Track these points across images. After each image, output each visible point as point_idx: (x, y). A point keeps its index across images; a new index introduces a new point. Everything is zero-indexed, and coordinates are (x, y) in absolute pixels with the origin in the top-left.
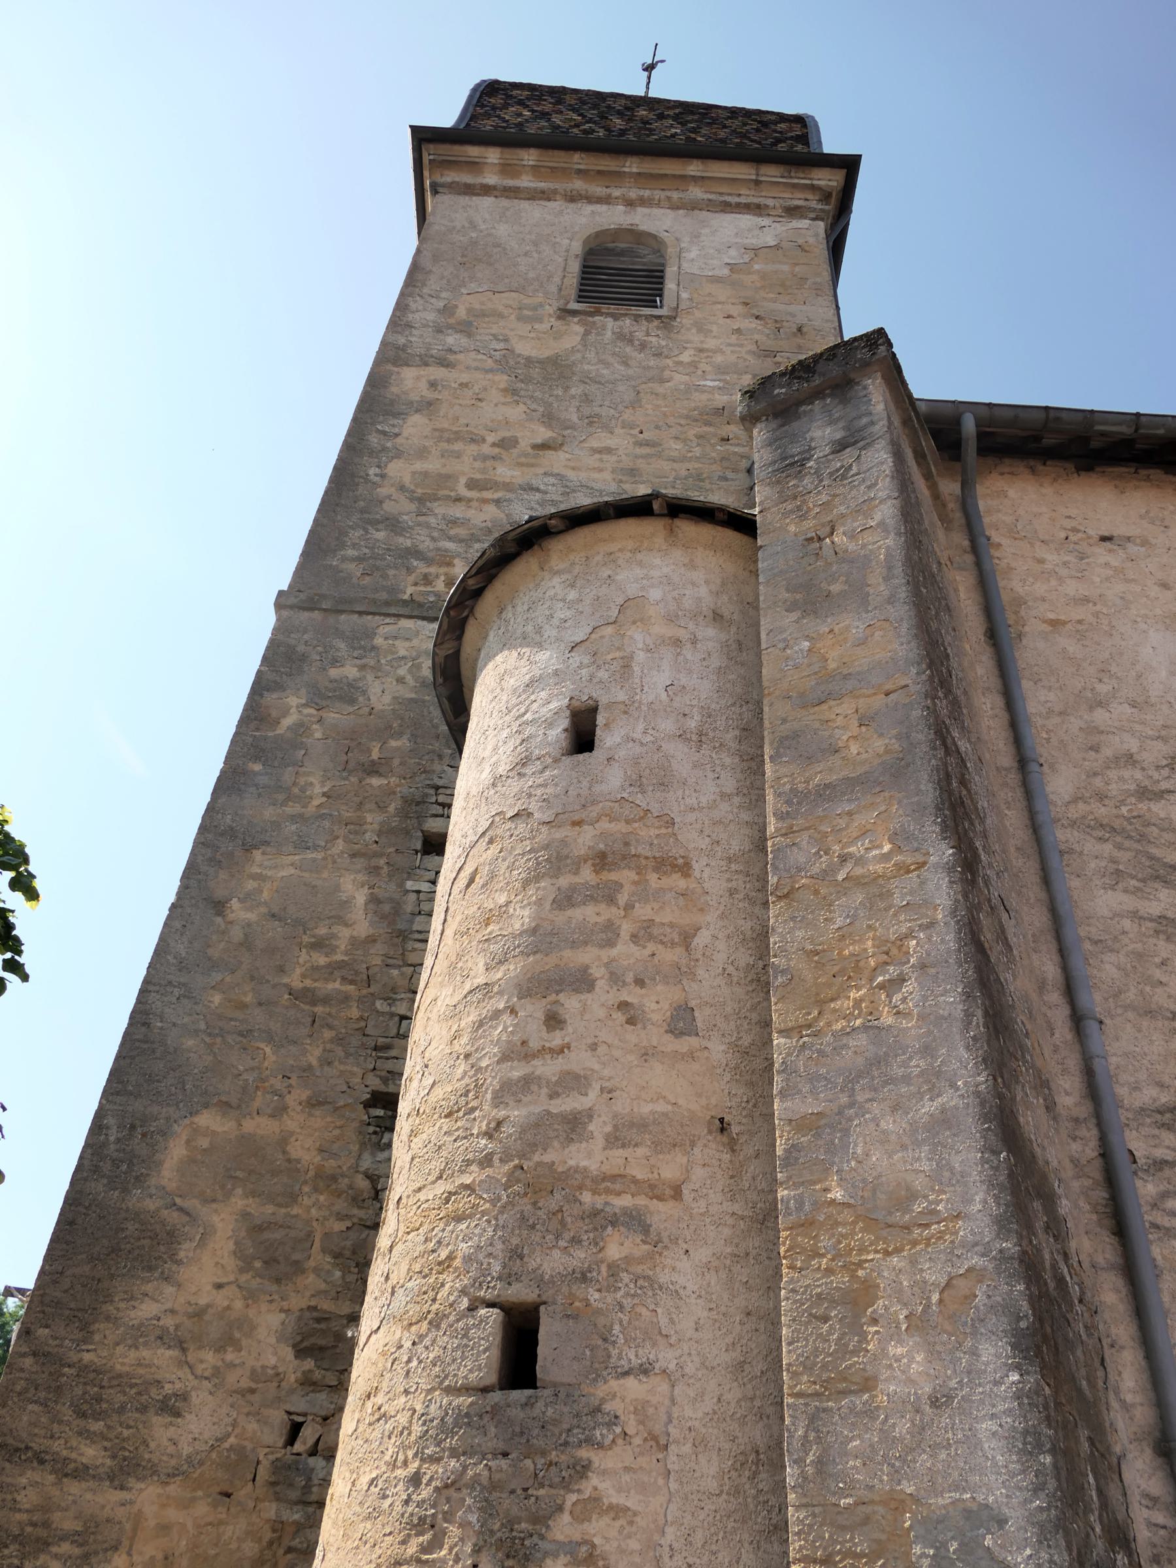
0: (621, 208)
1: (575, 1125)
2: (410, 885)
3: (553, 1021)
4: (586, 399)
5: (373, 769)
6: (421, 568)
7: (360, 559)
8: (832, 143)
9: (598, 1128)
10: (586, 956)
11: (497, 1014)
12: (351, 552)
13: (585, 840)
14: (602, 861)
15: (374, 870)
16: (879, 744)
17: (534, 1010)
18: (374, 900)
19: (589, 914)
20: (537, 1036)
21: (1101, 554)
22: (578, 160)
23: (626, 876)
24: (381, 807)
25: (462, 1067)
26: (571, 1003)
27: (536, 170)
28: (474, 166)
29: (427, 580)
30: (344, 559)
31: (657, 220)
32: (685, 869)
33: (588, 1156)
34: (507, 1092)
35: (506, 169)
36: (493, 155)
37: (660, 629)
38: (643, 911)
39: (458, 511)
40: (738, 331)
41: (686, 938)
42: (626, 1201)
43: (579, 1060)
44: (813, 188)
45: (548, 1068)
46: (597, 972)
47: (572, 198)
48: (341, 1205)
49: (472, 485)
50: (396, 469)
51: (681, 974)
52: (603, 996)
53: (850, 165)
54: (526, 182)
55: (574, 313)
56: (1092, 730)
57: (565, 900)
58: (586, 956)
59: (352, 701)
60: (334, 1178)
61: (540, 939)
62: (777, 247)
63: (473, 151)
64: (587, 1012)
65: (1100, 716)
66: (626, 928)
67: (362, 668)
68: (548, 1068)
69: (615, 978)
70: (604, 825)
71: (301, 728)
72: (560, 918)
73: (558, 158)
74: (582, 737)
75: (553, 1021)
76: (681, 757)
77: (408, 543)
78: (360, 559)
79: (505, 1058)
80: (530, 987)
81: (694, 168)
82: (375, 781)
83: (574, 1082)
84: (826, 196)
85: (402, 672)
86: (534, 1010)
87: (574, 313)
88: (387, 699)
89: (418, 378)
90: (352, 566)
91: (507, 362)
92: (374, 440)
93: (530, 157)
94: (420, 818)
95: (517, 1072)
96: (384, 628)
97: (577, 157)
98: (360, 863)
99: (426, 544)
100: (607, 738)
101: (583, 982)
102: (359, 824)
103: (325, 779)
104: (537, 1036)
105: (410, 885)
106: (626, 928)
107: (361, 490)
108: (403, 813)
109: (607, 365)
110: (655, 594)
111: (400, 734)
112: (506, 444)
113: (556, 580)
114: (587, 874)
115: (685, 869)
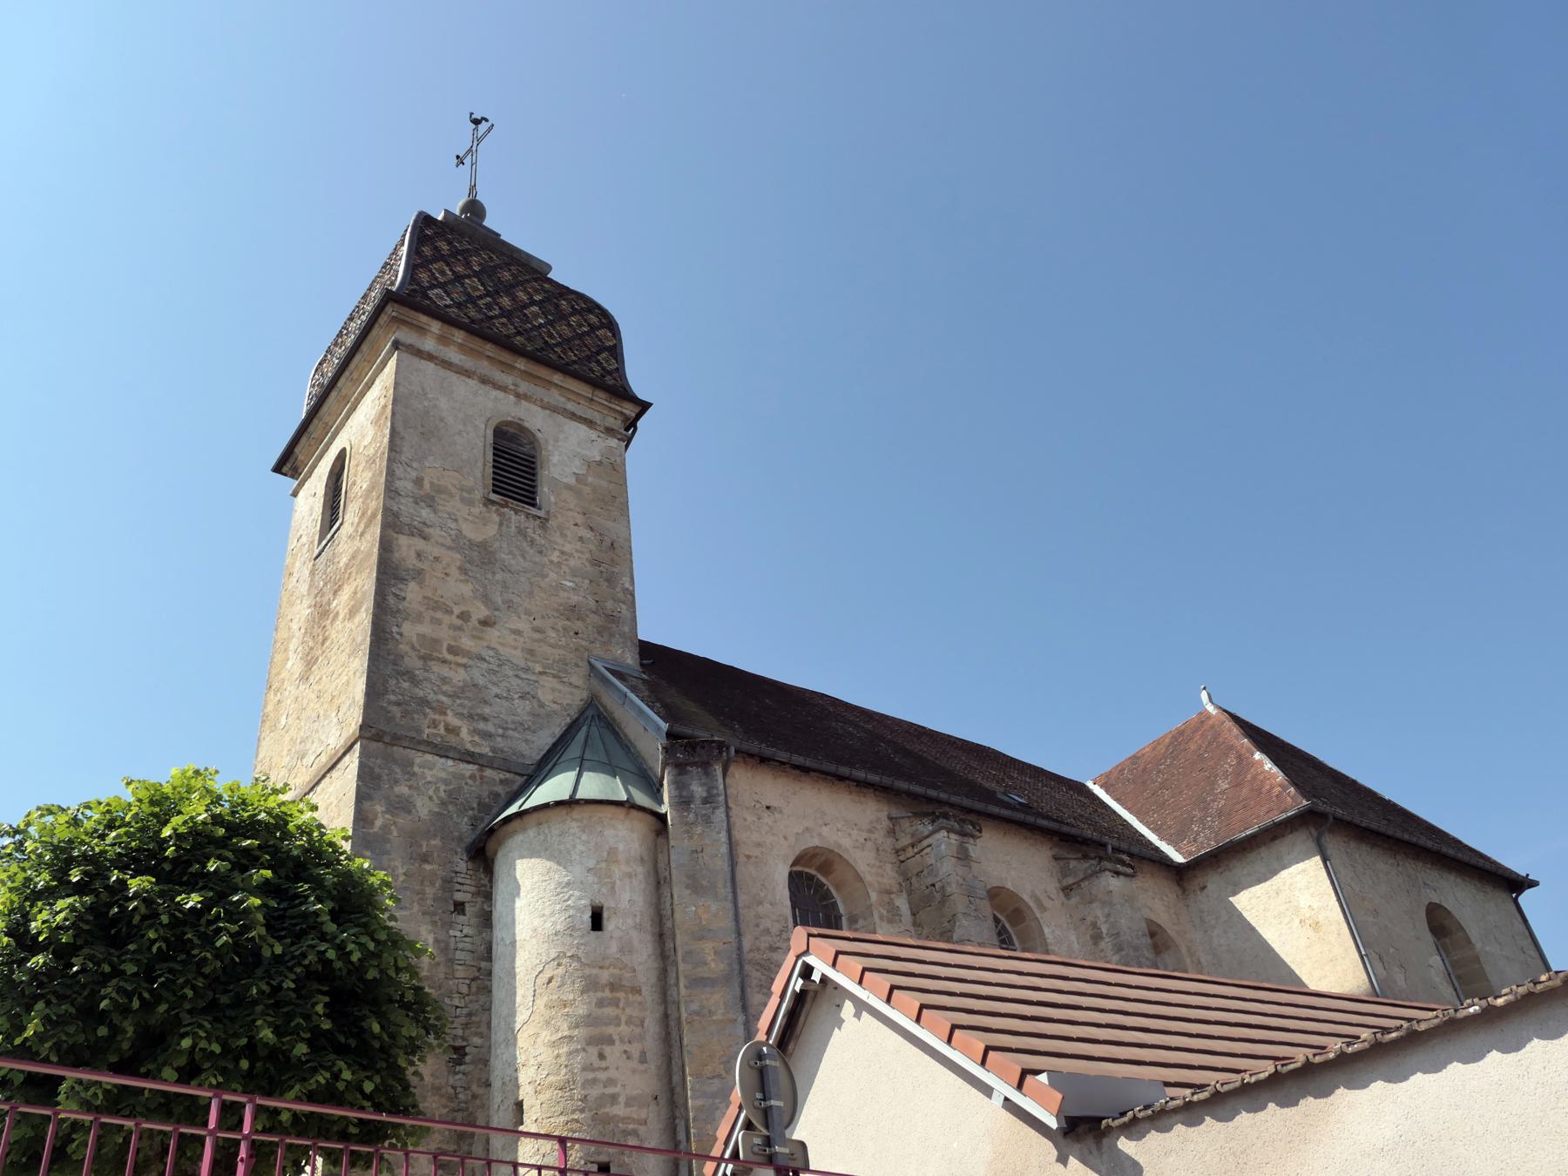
0: (512, 397)
1: (614, 1098)
2: (452, 933)
3: (602, 1056)
4: (505, 585)
5: (425, 859)
6: (432, 715)
7: (398, 704)
8: (640, 389)
9: (622, 1099)
10: (611, 1030)
11: (577, 1051)
12: (392, 697)
13: (605, 976)
14: (613, 987)
15: (434, 923)
16: (722, 966)
17: (593, 1051)
18: (436, 941)
19: (610, 1011)
20: (597, 1063)
21: (766, 814)
22: (490, 349)
23: (621, 995)
24: (433, 884)
25: (564, 1071)
26: (607, 1050)
27: (462, 348)
28: (422, 330)
29: (434, 724)
30: (390, 702)
31: (535, 419)
32: (639, 992)
33: (619, 1110)
34: (587, 1084)
35: (443, 340)
36: (435, 326)
37: (624, 868)
38: (628, 1011)
39: (445, 671)
40: (581, 539)
41: (642, 1023)
42: (631, 1126)
43: (612, 1073)
44: (621, 413)
45: (602, 1076)
46: (616, 1037)
47: (484, 381)
48: (444, 1101)
49: (451, 650)
50: (407, 627)
51: (641, 1038)
52: (618, 1048)
53: (644, 406)
54: (453, 355)
55: (493, 503)
56: (758, 916)
57: (601, 1004)
58: (611, 1030)
59: (409, 812)
60: (439, 1089)
61: (589, 1020)
62: (600, 463)
63: (423, 319)
64: (614, 1053)
65: (760, 909)
66: (623, 1019)
67: (410, 787)
68: (602, 1076)
69: (622, 1041)
70: (612, 970)
71: (385, 828)
72: (599, 1012)
73: (476, 343)
74: (597, 921)
75: (602, 1056)
76: (634, 934)
77: (421, 694)
78: (398, 704)
79: (584, 1069)
80: (592, 1041)
81: (557, 378)
82: (428, 867)
83: (611, 1082)
84: (626, 418)
85: (431, 792)
86: (593, 1051)
87: (493, 503)
88: (425, 811)
89: (409, 546)
90: (394, 709)
91: (458, 542)
92: (391, 600)
93: (459, 336)
94: (451, 891)
95: (590, 1076)
96: (419, 758)
97: (489, 346)
98: (428, 918)
99: (431, 697)
100: (610, 924)
101: (610, 1041)
102: (421, 893)
103: (403, 864)
104: (597, 1063)
105: (452, 933)
106: (623, 1019)
107: (391, 646)
108: (443, 888)
109: (514, 557)
110: (621, 847)
111: (435, 836)
112: (464, 616)
113: (574, 824)
114: (607, 993)
115: (639, 992)
